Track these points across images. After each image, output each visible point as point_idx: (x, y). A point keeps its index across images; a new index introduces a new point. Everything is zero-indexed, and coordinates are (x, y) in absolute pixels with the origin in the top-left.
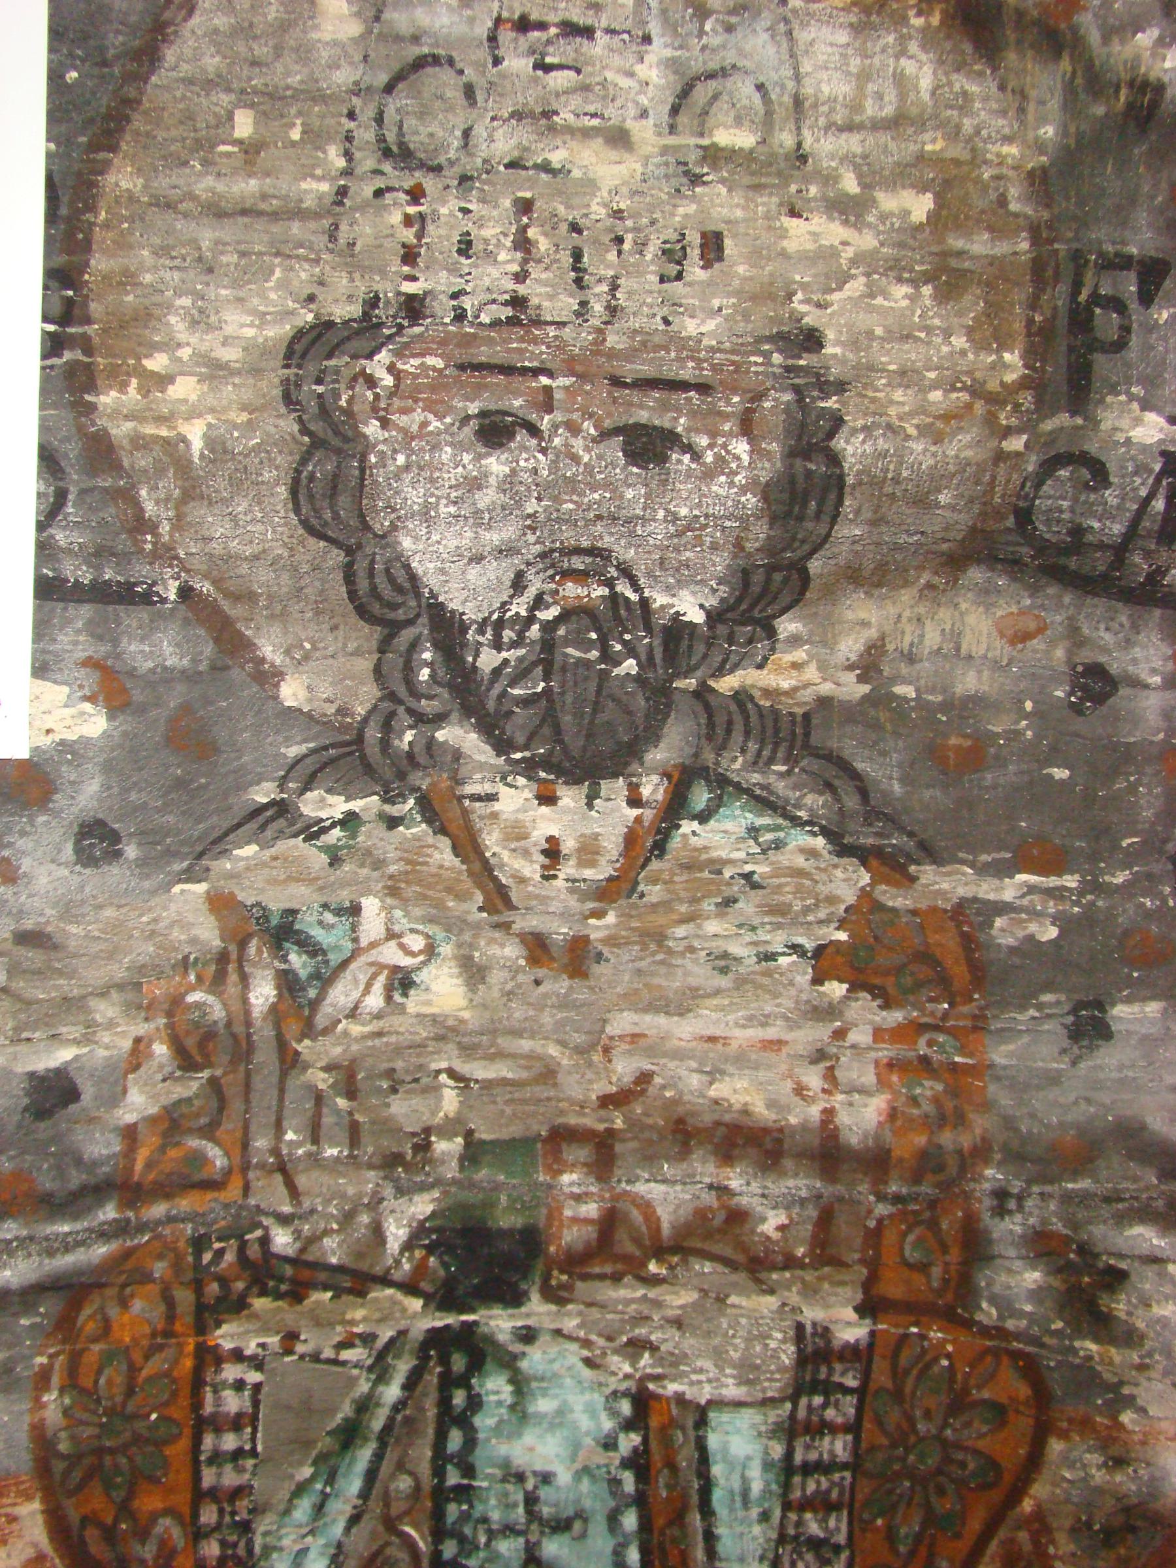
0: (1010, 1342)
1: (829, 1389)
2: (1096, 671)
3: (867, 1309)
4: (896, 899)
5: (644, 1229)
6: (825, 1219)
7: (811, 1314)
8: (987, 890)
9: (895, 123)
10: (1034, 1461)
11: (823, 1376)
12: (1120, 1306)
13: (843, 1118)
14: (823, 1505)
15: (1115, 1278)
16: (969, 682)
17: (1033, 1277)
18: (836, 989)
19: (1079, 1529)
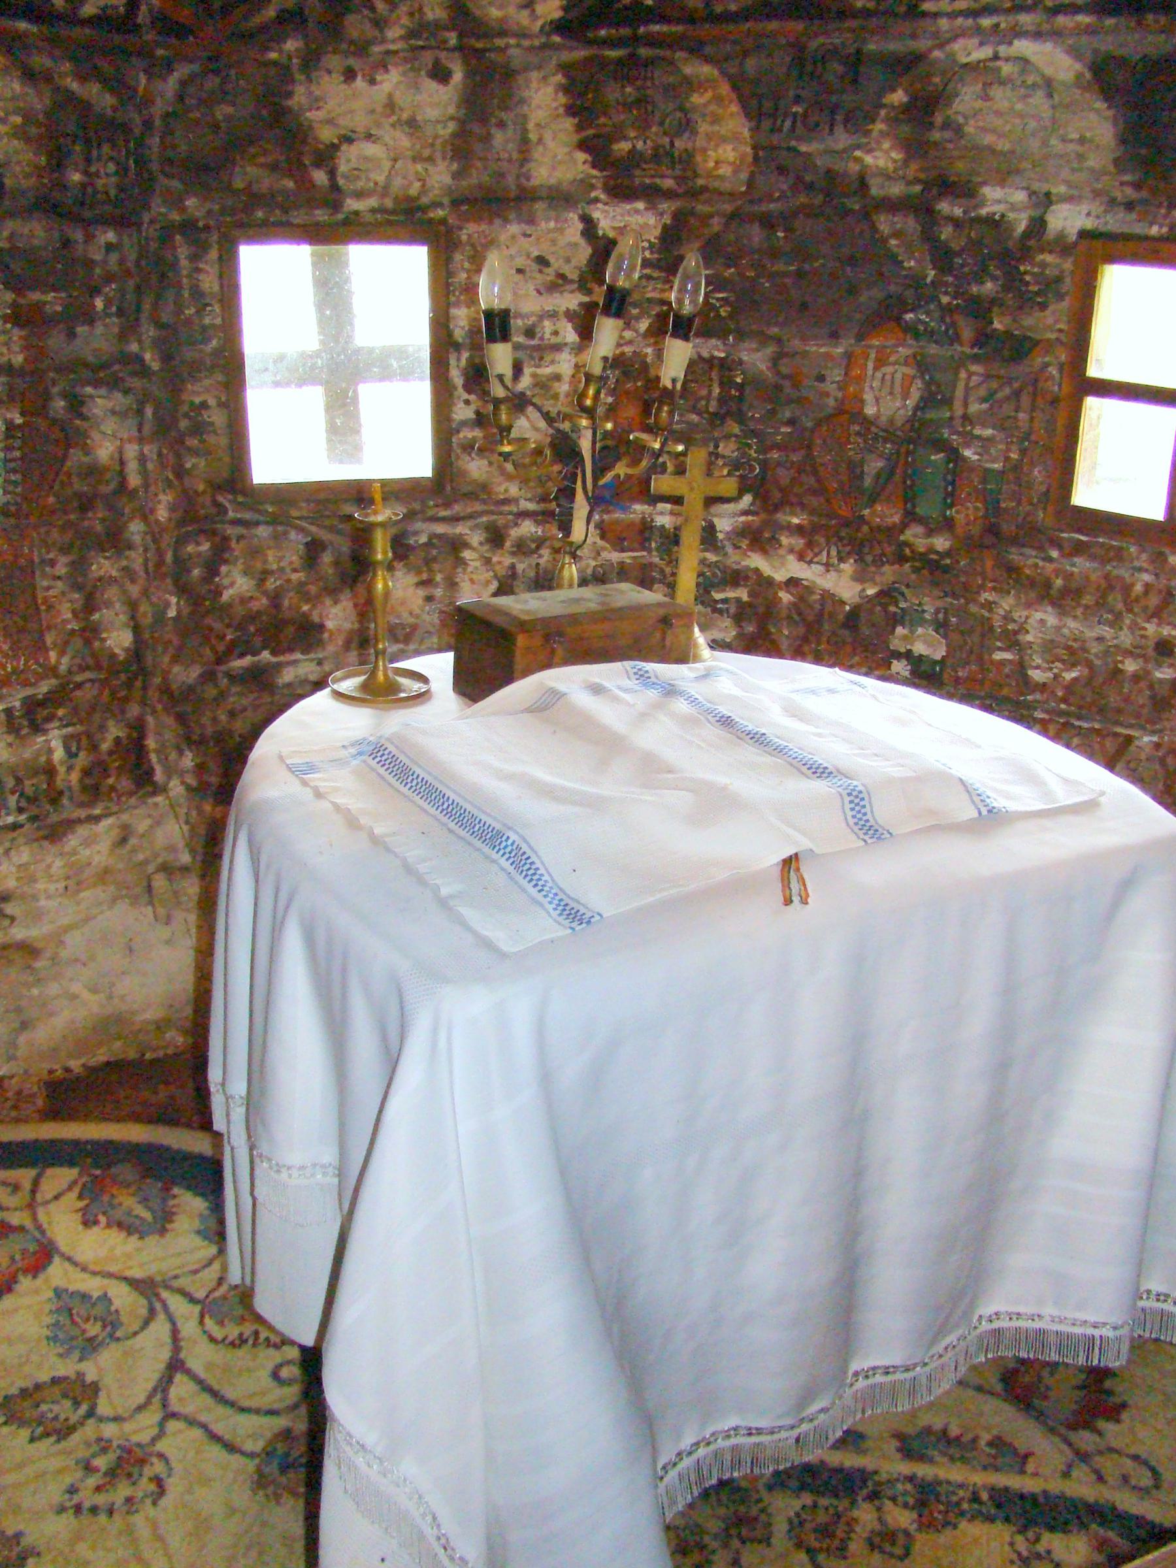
0: (967, 445)
1: (13, 437)
2: (68, 240)
3: (23, 414)
4: (22, 301)
5: (514, 187)
6: (11, 389)
7: (9, 416)
8: (44, 298)
9: (13, 99)
10: (65, 457)
11: (785, 540)
12: (84, 410)
13: (14, 361)
14: (15, 471)
15: (82, 403)
16: (36, 242)
17: (62, 403)
18: (9, 326)
19: (79, 475)
